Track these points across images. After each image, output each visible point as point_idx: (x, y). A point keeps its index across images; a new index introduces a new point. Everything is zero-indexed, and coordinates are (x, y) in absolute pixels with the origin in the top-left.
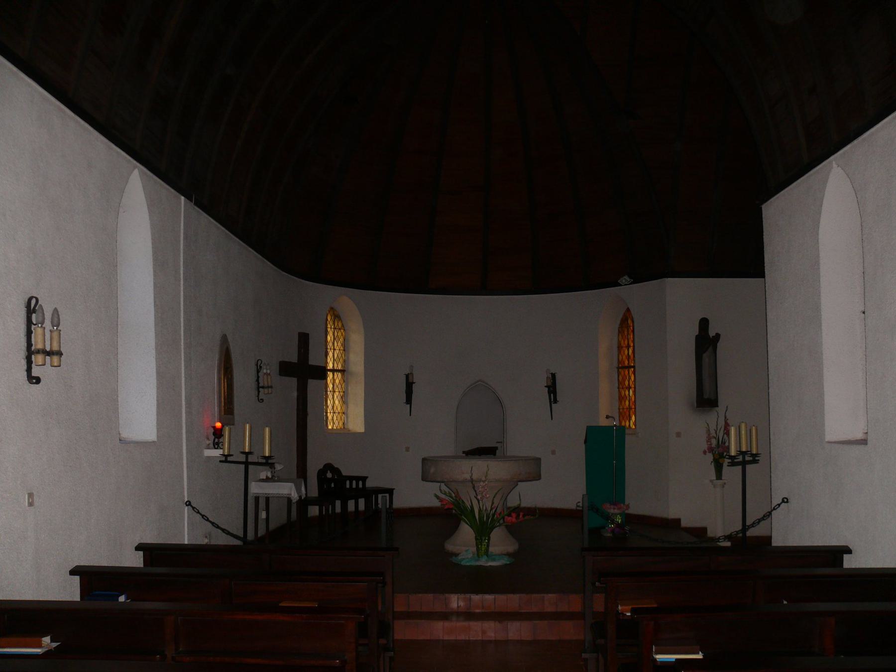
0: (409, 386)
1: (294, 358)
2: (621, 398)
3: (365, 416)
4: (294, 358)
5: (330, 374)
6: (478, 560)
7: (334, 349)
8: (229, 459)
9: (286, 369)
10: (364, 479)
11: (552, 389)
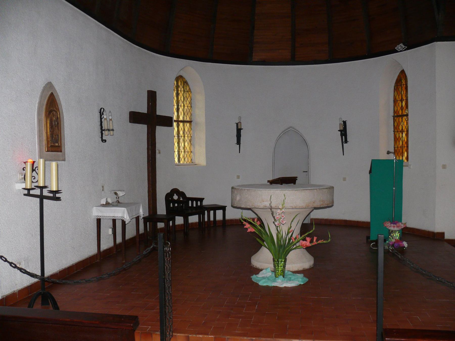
0: (239, 131)
1: (143, 109)
2: (396, 140)
3: (207, 153)
4: (143, 109)
5: (175, 124)
6: (274, 281)
7: (184, 106)
8: (32, 192)
9: (135, 117)
10: (201, 200)
11: (344, 132)
